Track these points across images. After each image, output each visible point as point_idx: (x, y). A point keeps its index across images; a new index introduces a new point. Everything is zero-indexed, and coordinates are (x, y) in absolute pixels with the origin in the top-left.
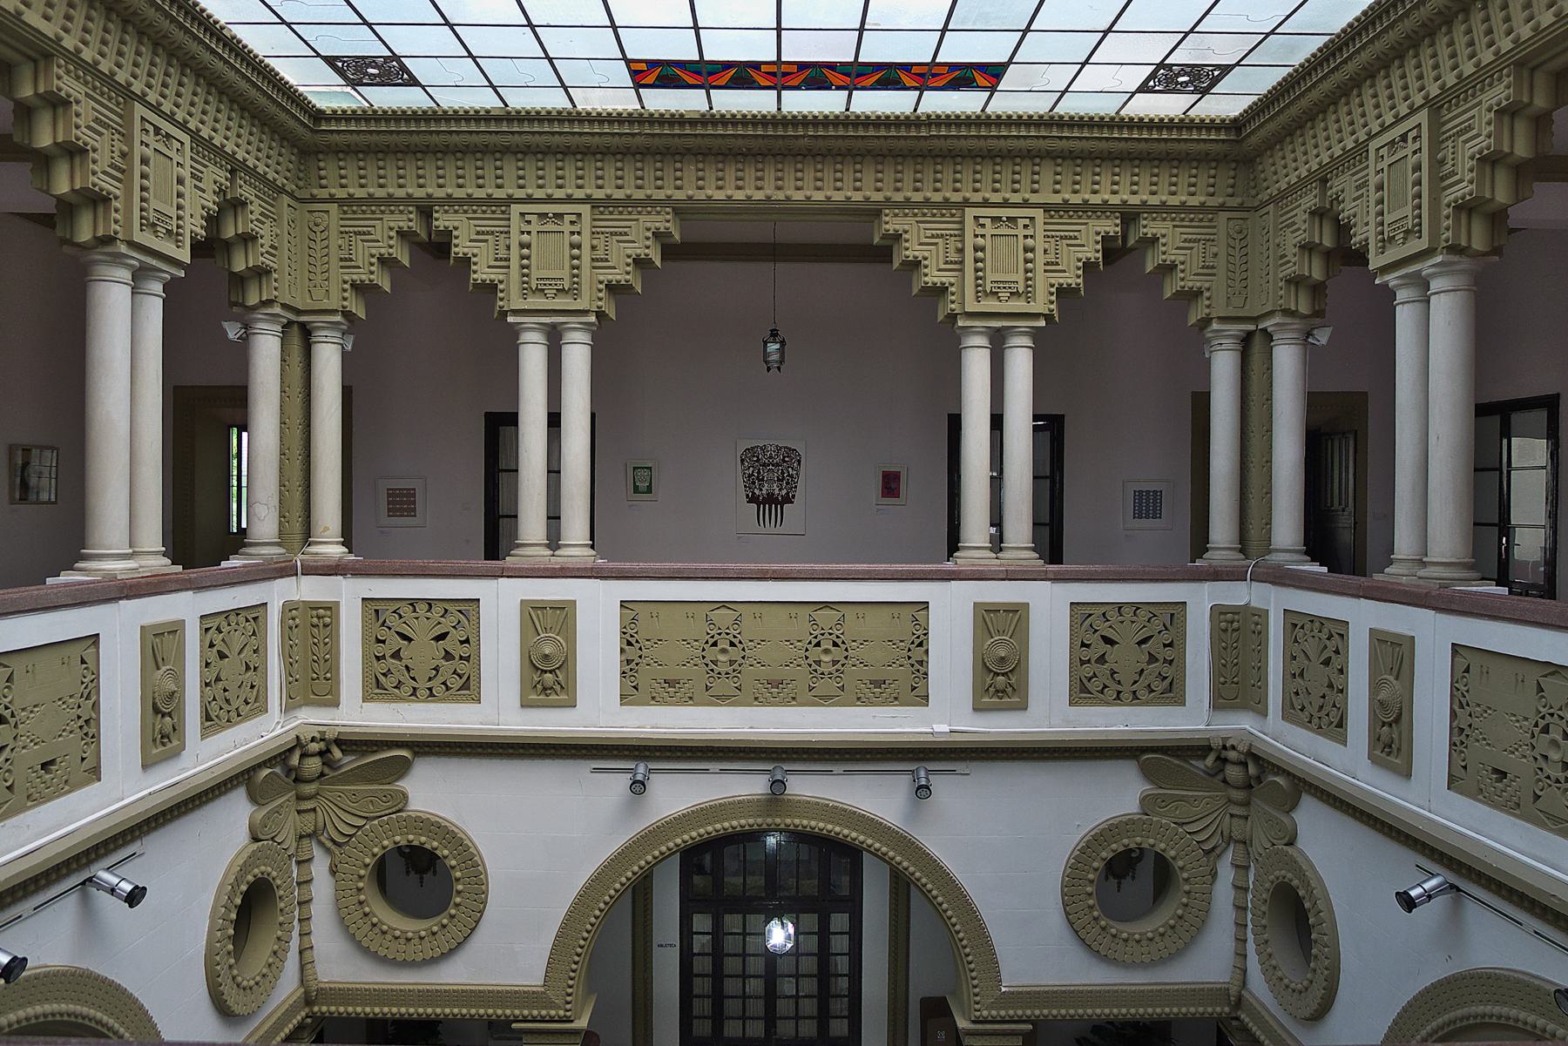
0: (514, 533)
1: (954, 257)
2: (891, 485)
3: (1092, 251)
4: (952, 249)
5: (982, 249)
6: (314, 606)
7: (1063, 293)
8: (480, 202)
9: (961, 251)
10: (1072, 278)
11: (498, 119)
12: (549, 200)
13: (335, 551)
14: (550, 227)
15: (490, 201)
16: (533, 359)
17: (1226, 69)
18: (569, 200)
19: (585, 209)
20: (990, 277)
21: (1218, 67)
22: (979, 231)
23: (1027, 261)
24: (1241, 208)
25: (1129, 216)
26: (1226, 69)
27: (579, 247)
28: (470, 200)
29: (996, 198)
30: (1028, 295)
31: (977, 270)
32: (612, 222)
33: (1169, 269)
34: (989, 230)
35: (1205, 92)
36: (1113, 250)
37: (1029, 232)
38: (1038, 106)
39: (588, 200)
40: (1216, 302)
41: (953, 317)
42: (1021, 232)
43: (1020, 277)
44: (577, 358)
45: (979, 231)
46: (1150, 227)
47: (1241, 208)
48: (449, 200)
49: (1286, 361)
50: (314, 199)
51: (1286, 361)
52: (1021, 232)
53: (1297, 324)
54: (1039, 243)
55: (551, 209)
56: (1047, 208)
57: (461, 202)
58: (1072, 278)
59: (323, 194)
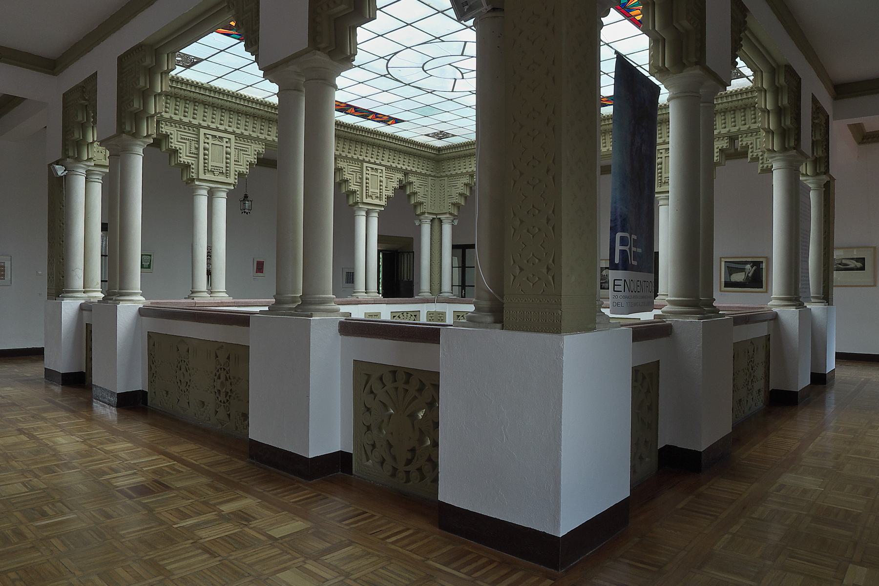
0: (420, 289)
1: (193, 150)
2: (260, 267)
3: (396, 185)
4: (193, 147)
5: (208, 150)
6: (439, 313)
7: (240, 175)
8: (185, 124)
9: (198, 149)
10: (244, 169)
11: (206, 89)
12: (217, 130)
13: (427, 295)
14: (217, 142)
15: (189, 125)
16: (202, 202)
17: (200, 60)
18: (225, 131)
19: (232, 137)
20: (211, 163)
21: (196, 58)
22: (206, 141)
23: (227, 158)
24: (434, 176)
25: (406, 173)
26: (200, 60)
27: (230, 154)
28: (180, 122)
29: (213, 126)
30: (227, 175)
31: (205, 159)
32: (243, 145)
33: (415, 193)
34: (210, 141)
35: (188, 67)
36: (402, 187)
37: (228, 145)
38: (202, 79)
39: (233, 133)
40: (427, 207)
41: (357, 203)
42: (225, 145)
43: (224, 165)
44: (221, 204)
45: (206, 141)
46: (412, 179)
47: (434, 176)
48: (170, 121)
49: (447, 229)
50: (441, 177)
51: (447, 229)
52: (225, 145)
53: (452, 218)
54: (384, 179)
55: (375, 166)
56: (238, 136)
57: (175, 122)
58: (244, 169)
59: (444, 174)
